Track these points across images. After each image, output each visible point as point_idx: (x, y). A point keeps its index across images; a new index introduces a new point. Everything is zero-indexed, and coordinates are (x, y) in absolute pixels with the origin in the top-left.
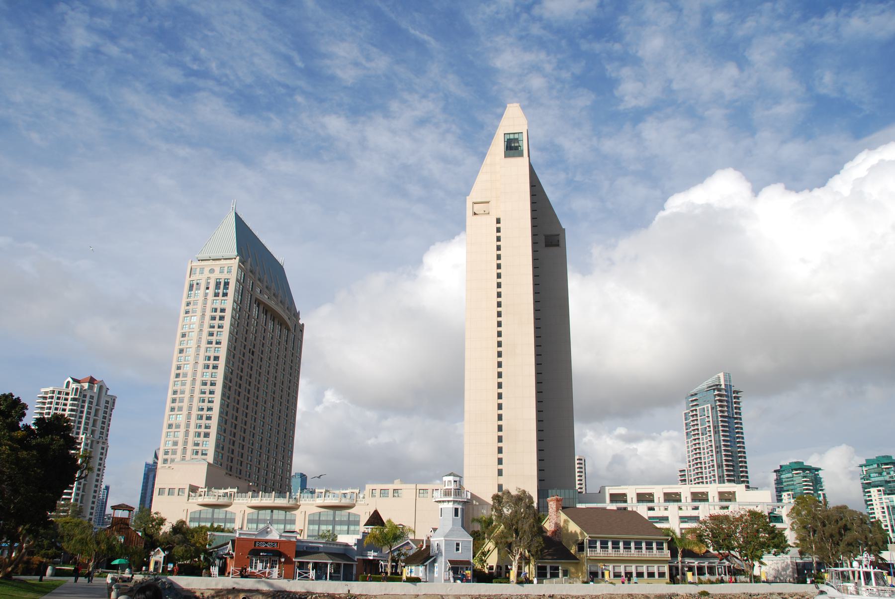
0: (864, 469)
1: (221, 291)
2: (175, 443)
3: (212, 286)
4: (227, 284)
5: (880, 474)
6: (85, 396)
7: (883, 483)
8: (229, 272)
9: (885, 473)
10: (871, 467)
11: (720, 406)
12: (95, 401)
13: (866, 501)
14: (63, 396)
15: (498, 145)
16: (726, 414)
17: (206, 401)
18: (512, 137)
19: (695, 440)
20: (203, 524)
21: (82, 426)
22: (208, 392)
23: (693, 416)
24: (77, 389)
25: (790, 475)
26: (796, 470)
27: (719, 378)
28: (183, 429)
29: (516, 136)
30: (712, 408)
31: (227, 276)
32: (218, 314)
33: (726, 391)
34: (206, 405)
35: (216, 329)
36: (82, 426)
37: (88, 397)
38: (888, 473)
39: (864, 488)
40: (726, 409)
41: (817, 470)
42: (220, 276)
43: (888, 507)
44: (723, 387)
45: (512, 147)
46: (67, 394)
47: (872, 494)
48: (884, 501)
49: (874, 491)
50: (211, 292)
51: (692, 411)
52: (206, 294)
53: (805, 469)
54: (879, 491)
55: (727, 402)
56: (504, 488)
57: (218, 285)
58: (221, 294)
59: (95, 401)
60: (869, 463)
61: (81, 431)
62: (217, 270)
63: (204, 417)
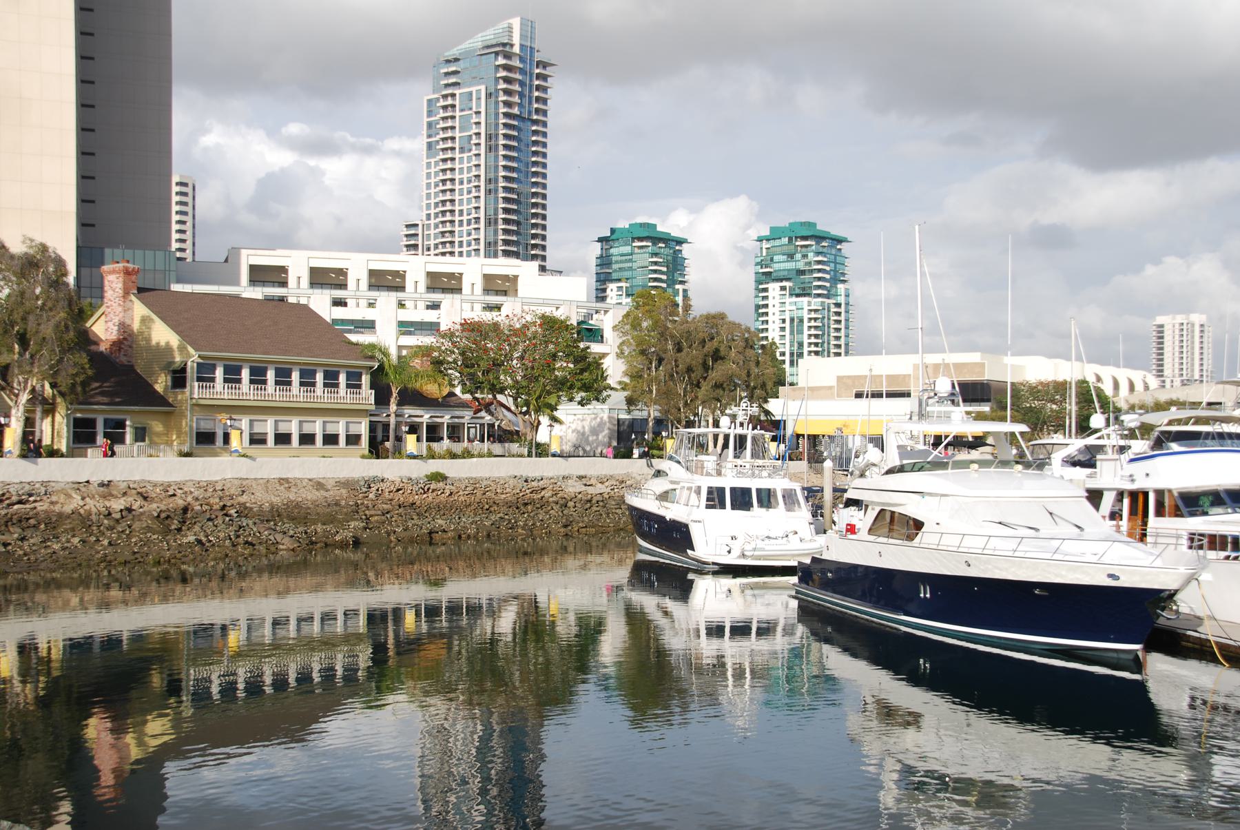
0: (765, 245)
5: (791, 256)
7: (793, 275)
9: (798, 256)
10: (777, 243)
16: (516, 111)
23: (445, 108)
25: (627, 249)
30: (489, 95)
33: (522, 60)
39: (759, 282)
41: (680, 242)
43: (792, 320)
44: (516, 49)
47: (770, 294)
49: (774, 288)
51: (445, 97)
54: (783, 288)
55: (522, 84)
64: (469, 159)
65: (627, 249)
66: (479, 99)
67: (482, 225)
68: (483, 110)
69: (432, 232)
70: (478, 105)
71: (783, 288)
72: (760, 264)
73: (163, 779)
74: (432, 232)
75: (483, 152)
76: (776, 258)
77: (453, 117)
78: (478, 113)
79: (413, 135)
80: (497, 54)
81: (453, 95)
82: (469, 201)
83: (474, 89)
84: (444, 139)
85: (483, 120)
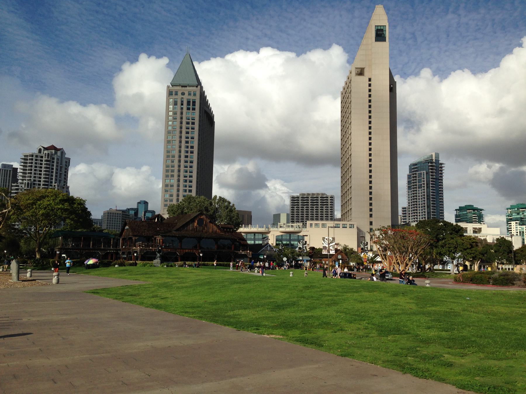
0: (509, 211)
1: (191, 107)
2: (171, 196)
3: (185, 103)
4: (194, 103)
5: (518, 214)
6: (53, 159)
7: (519, 219)
8: (195, 95)
9: (521, 214)
10: (513, 210)
11: (432, 172)
12: (59, 161)
13: (508, 228)
14: (39, 158)
15: (372, 34)
16: (434, 177)
17: (188, 172)
18: (379, 28)
19: (414, 191)
20: (257, 242)
21: (54, 177)
22: (189, 167)
23: (413, 177)
24: (48, 154)
25: (466, 212)
26: (469, 210)
27: (432, 156)
28: (175, 188)
29: (382, 28)
30: (427, 173)
31: (194, 98)
32: (191, 121)
33: (435, 163)
34: (188, 174)
35: (190, 130)
36: (54, 177)
37: (55, 159)
38: (523, 214)
39: (507, 221)
40: (434, 174)
41: (481, 210)
42: (189, 97)
43: (520, 232)
44: (434, 161)
45: (380, 35)
46: (42, 157)
47: (512, 225)
48: (518, 228)
49: (513, 223)
50: (185, 106)
51: (413, 174)
52: (182, 108)
53: (474, 209)
54: (516, 223)
55: (436, 170)
56: (150, 208)
57: (188, 103)
58: (191, 109)
59: (59, 161)
60: (512, 207)
61: (54, 181)
62: (187, 93)
63: (188, 181)
64: (421, 190)
65: (466, 212)
66: (424, 174)
67: (426, 208)
68: (425, 177)
69: (410, 210)
70: (424, 176)
71: (516, 223)
72: (508, 216)
73: (326, 47)
74: (410, 210)
75: (425, 188)
76: (513, 214)
77: (416, 180)
78: (424, 178)
79: (501, 214)
80: (429, 162)
81: (416, 174)
82: (422, 201)
83: (422, 172)
84: (413, 185)
85: (425, 180)
